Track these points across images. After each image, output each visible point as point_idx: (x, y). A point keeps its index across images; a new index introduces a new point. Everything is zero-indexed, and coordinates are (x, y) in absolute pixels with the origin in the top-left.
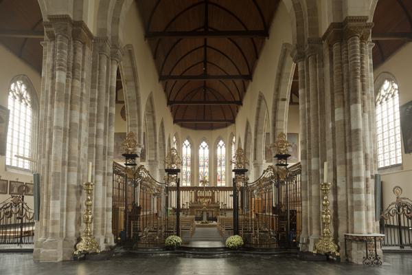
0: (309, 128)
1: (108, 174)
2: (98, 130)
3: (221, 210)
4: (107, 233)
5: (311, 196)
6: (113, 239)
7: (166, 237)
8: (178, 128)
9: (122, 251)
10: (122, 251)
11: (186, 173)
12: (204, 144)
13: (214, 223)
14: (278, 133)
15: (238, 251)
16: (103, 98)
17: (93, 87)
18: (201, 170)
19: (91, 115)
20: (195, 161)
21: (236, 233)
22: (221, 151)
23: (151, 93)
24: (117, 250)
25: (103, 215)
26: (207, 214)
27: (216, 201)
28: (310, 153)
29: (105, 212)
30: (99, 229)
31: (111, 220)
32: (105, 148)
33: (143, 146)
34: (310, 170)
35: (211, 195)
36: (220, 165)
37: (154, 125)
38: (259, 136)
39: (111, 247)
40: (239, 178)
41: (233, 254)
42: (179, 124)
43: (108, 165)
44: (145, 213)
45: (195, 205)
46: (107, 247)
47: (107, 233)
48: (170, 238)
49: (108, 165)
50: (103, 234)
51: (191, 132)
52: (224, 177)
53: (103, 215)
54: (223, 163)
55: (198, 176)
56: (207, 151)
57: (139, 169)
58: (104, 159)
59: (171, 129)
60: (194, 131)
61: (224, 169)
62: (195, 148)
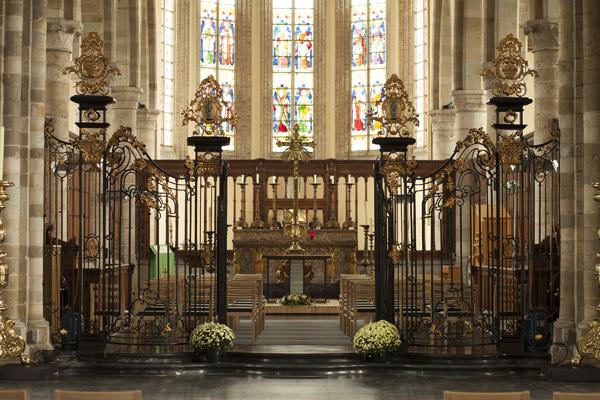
0: (580, 29)
1: (34, 153)
3: (360, 254)
4: (31, 318)
5: (581, 213)
7: (189, 328)
10: (76, 363)
13: (334, 303)
14: (501, 35)
15: (388, 364)
18: (280, 77)
20: (255, 38)
21: (383, 312)
25: (23, 267)
26: (306, 270)
27: (342, 219)
28: (580, 98)
29: (27, 258)
30: (15, 304)
31: (41, 280)
32: (25, 79)
34: (580, 143)
35: (320, 195)
36: (366, 58)
39: (44, 353)
41: (374, 365)
45: (256, 237)
46: (33, 355)
48: (205, 327)
49: (33, 129)
50: (23, 320)
53: (23, 267)
55: (267, 106)
57: (116, 138)
58: (24, 113)
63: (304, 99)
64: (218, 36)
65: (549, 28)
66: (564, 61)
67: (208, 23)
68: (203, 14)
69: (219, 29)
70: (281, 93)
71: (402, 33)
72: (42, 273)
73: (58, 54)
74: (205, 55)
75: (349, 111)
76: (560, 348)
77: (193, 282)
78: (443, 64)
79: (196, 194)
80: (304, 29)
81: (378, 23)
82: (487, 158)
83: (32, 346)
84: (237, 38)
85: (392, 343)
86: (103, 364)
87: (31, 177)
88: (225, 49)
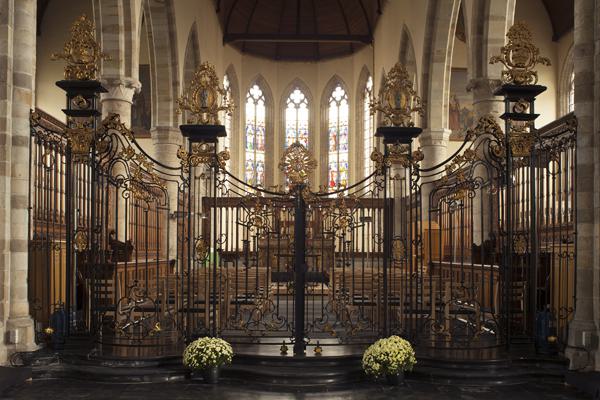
6: (31, 332)
8: (235, 56)
9: (57, 366)
10: (57, 366)
11: (255, 166)
12: (297, 95)
22: (339, 113)
23: (195, 23)
24: (39, 365)
33: (138, 85)
37: (172, 36)
38: (435, 66)
39: (22, 355)
40: (396, 154)
42: (236, 46)
43: (15, 115)
44: (142, 261)
46: (11, 357)
47: (12, 316)
49: (15, 115)
51: (265, 66)
54: (343, 141)
56: (304, 113)
59: (216, 54)
60: (276, 65)
61: (344, 156)
62: (275, 106)
64: (255, 134)
65: (488, 84)
66: (583, 45)
67: (250, 127)
68: (247, 122)
69: (256, 131)
71: (357, 133)
72: (26, 268)
73: (120, 103)
74: (248, 145)
75: (328, 176)
76: (581, 353)
77: (186, 280)
79: (189, 186)
80: (303, 132)
81: (344, 128)
82: (498, 149)
83: (11, 347)
84: (266, 136)
85: (407, 360)
86: (82, 369)
87: (13, 166)
88: (260, 142)
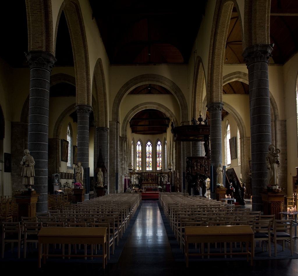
2: (122, 163)
16: (123, 154)
17: (121, 151)
18: (147, 160)
19: (121, 159)
20: (144, 154)
36: (159, 157)
52: (160, 164)
54: (160, 155)
58: (124, 171)
61: (161, 159)
63: (151, 163)
69: (139, 153)
70: (148, 162)
78: (269, 8)
80: (150, 153)
